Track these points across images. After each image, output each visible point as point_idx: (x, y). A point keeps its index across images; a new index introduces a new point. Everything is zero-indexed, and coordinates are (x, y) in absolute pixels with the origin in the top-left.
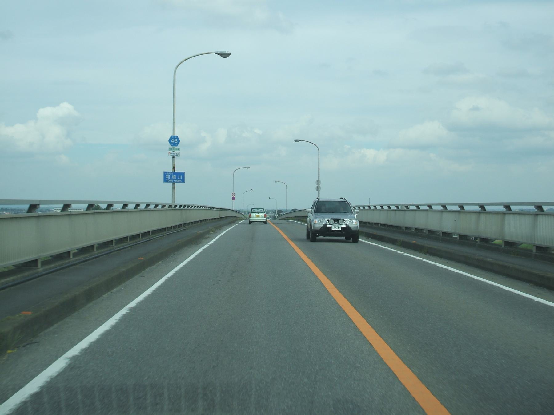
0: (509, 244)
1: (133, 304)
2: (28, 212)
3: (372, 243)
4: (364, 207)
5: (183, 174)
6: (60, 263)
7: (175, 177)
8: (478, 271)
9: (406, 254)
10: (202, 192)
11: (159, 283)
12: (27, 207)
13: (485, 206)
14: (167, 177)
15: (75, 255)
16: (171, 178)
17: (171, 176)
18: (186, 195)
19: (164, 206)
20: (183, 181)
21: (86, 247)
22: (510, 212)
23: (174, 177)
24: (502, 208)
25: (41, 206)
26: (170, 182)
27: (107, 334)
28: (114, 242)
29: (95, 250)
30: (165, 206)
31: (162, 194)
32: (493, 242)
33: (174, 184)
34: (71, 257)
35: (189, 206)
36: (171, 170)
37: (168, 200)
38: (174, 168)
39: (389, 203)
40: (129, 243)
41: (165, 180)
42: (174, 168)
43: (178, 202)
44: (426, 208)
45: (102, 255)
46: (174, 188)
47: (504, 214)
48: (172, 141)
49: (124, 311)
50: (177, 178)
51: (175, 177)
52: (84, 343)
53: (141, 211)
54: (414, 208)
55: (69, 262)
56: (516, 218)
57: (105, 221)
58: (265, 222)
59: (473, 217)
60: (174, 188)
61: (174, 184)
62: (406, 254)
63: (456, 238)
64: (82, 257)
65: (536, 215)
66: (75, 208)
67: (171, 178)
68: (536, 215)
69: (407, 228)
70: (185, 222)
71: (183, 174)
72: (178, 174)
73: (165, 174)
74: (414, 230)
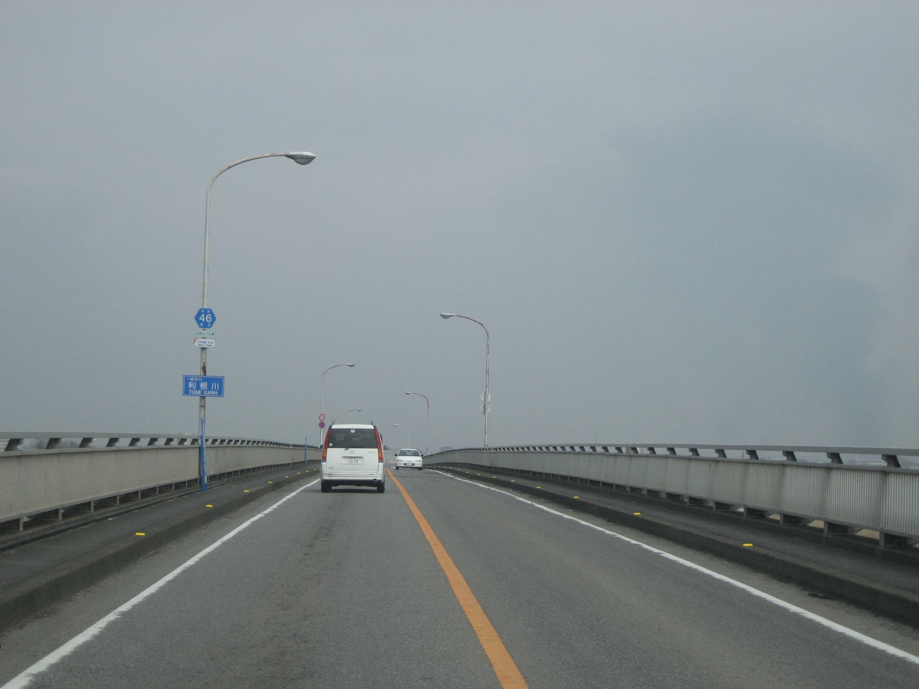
0: (789, 519)
1: (126, 607)
2: (47, 448)
3: (583, 522)
4: (605, 448)
5: (220, 380)
6: (37, 529)
7: (205, 385)
8: (717, 562)
9: (619, 536)
10: (257, 415)
11: (170, 577)
12: (79, 441)
13: (758, 452)
14: (190, 385)
15: (27, 525)
16: (198, 388)
17: (198, 383)
18: (226, 419)
19: (183, 440)
20: (220, 393)
21: (48, 512)
22: (756, 461)
23: (203, 385)
24: (879, 462)
25: (63, 440)
26: (196, 395)
27: (86, 645)
28: (93, 504)
29: (60, 517)
30: (216, 440)
31: (180, 417)
32: (859, 534)
33: (203, 398)
34: (21, 528)
35: (243, 441)
36: (199, 372)
37: (190, 431)
38: (204, 369)
39: (605, 442)
40: (118, 507)
41: (186, 391)
42: (204, 369)
43: (211, 432)
44: (712, 454)
45: (72, 528)
46: (203, 406)
47: (783, 465)
48: (208, 317)
49: (111, 617)
50: (209, 388)
51: (205, 385)
52: (53, 658)
53: (159, 449)
54: (687, 453)
55: (17, 538)
56: (850, 478)
57: (79, 467)
58: (378, 486)
59: (816, 477)
60: (203, 406)
61: (203, 398)
62: (619, 536)
63: (711, 508)
64: (38, 530)
65: (884, 473)
66: (26, 446)
67: (198, 388)
68: (884, 473)
69: (633, 489)
70: (223, 471)
71: (220, 380)
72: (210, 381)
73: (187, 380)
74: (645, 492)
